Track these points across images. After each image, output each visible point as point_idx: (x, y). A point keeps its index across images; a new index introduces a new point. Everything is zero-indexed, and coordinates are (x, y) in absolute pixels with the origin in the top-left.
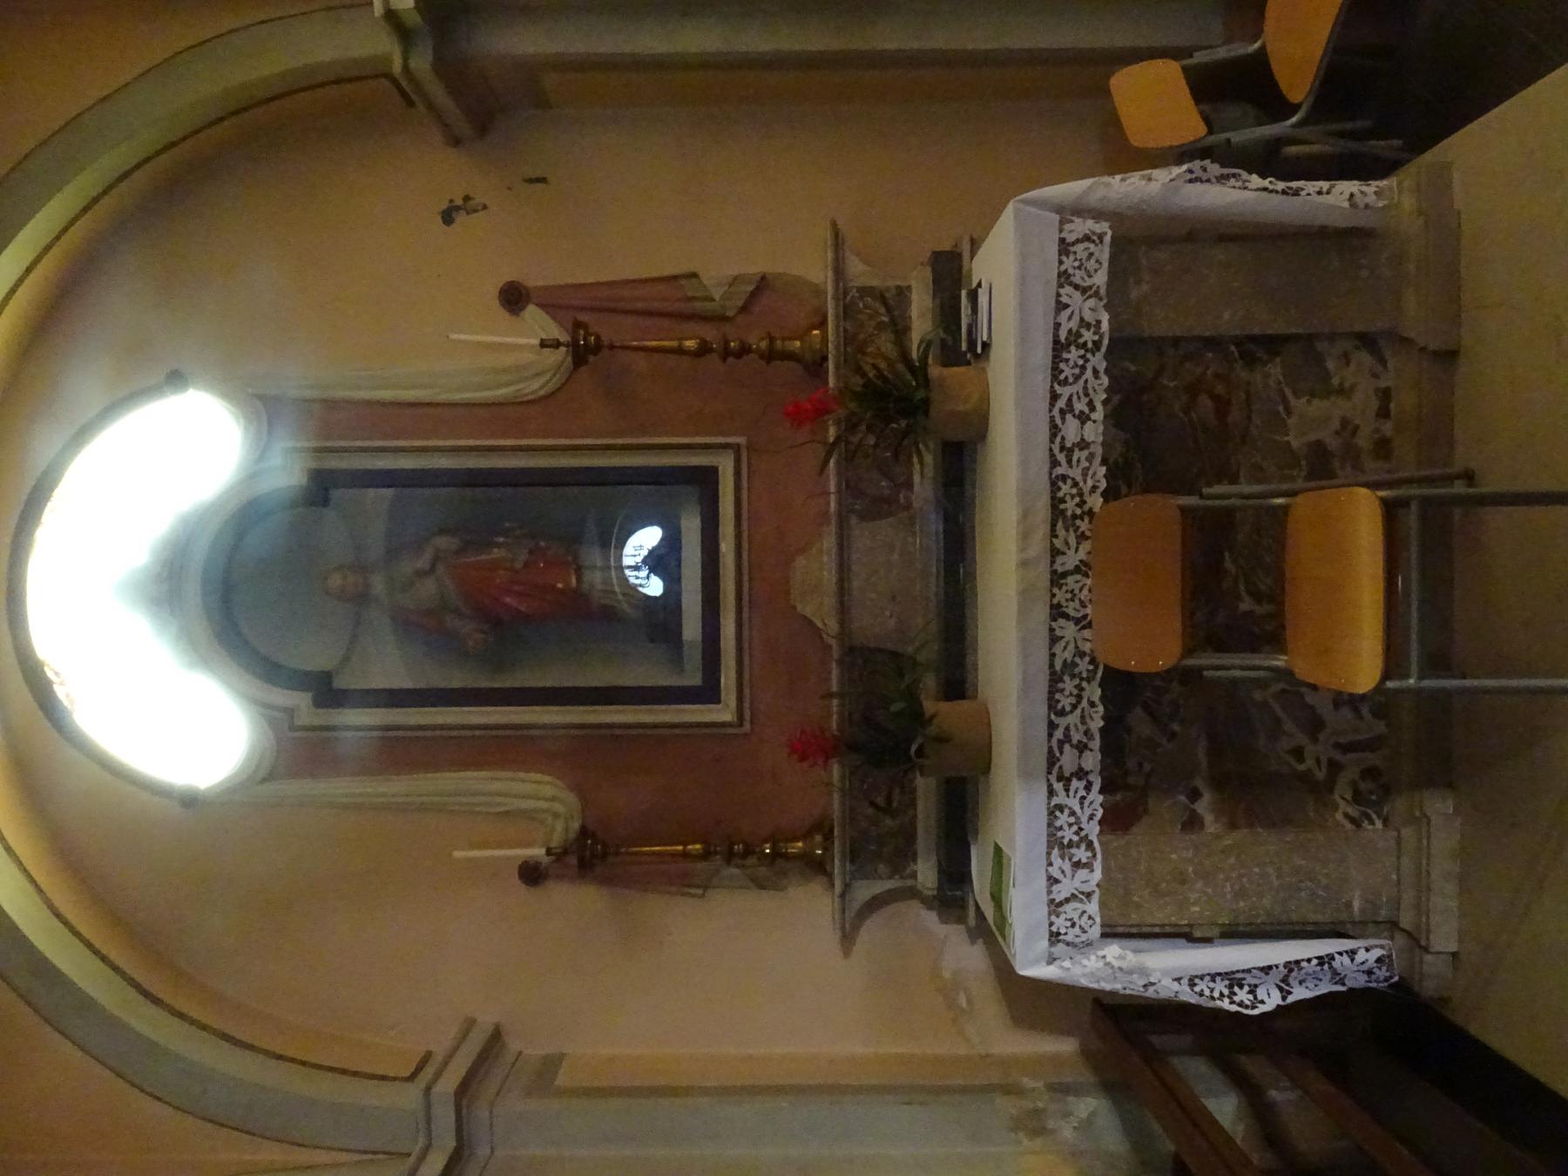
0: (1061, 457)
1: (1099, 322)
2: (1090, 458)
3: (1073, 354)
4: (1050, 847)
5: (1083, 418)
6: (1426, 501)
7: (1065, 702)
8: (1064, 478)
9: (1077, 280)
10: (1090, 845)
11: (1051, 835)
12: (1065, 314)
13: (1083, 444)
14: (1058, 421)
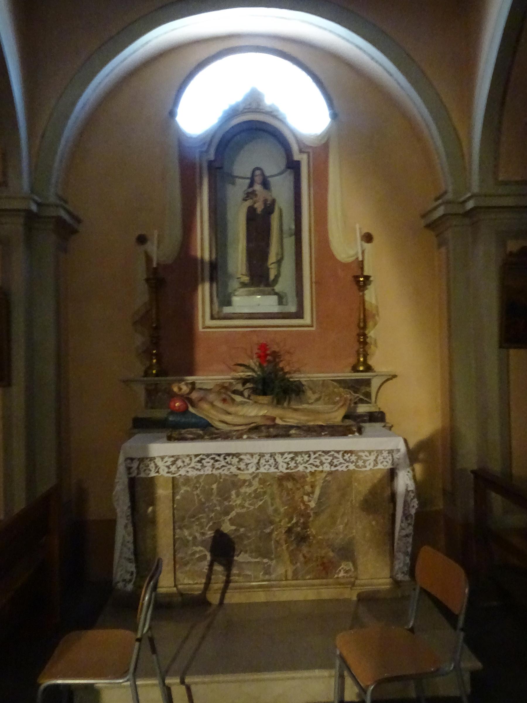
0: (317, 455)
1: (366, 467)
5: (331, 464)
7: (347, 457)
9: (141, 466)
12: (367, 454)
13: (203, 466)
14: (210, 457)
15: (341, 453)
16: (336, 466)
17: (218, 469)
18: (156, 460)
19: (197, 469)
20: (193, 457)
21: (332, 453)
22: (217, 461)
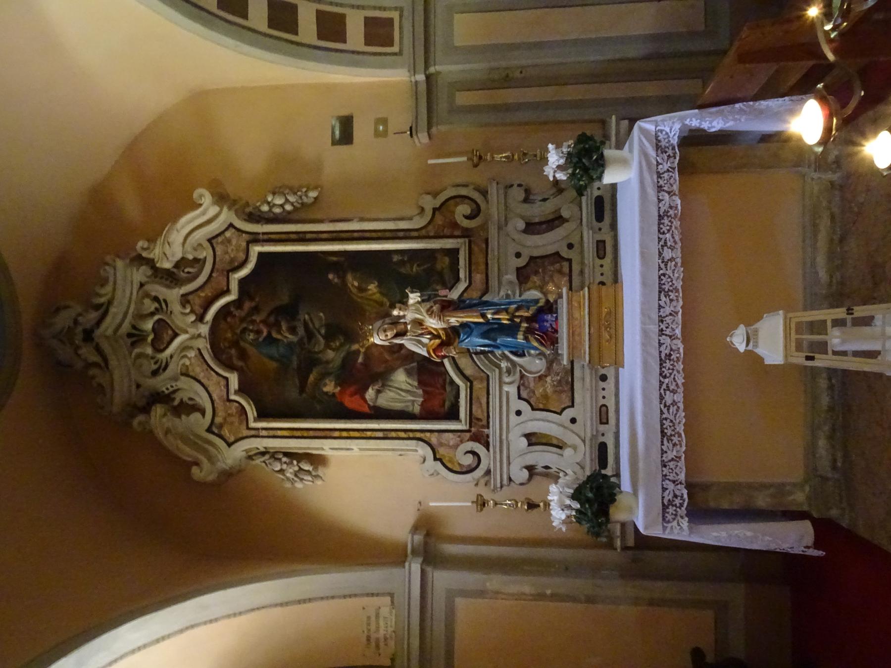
2: (675, 266)
3: (671, 510)
4: (660, 292)
6: (797, 332)
7: (665, 229)
8: (666, 419)
10: (680, 435)
11: (660, 288)
13: (674, 403)
15: (661, 236)
16: (675, 242)
17: (675, 242)
18: (663, 315)
19: (677, 411)
20: (661, 272)
21: (662, 391)
22: (665, 243)
